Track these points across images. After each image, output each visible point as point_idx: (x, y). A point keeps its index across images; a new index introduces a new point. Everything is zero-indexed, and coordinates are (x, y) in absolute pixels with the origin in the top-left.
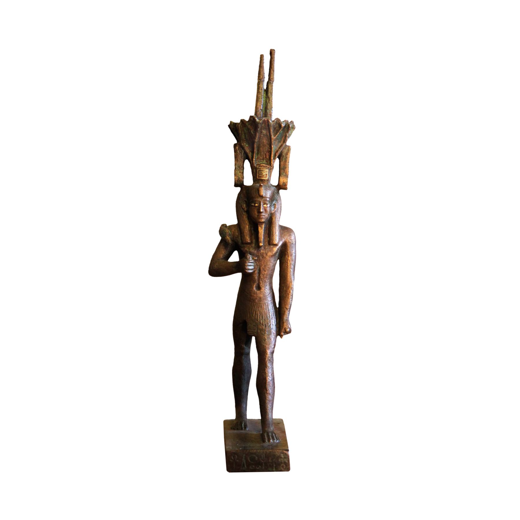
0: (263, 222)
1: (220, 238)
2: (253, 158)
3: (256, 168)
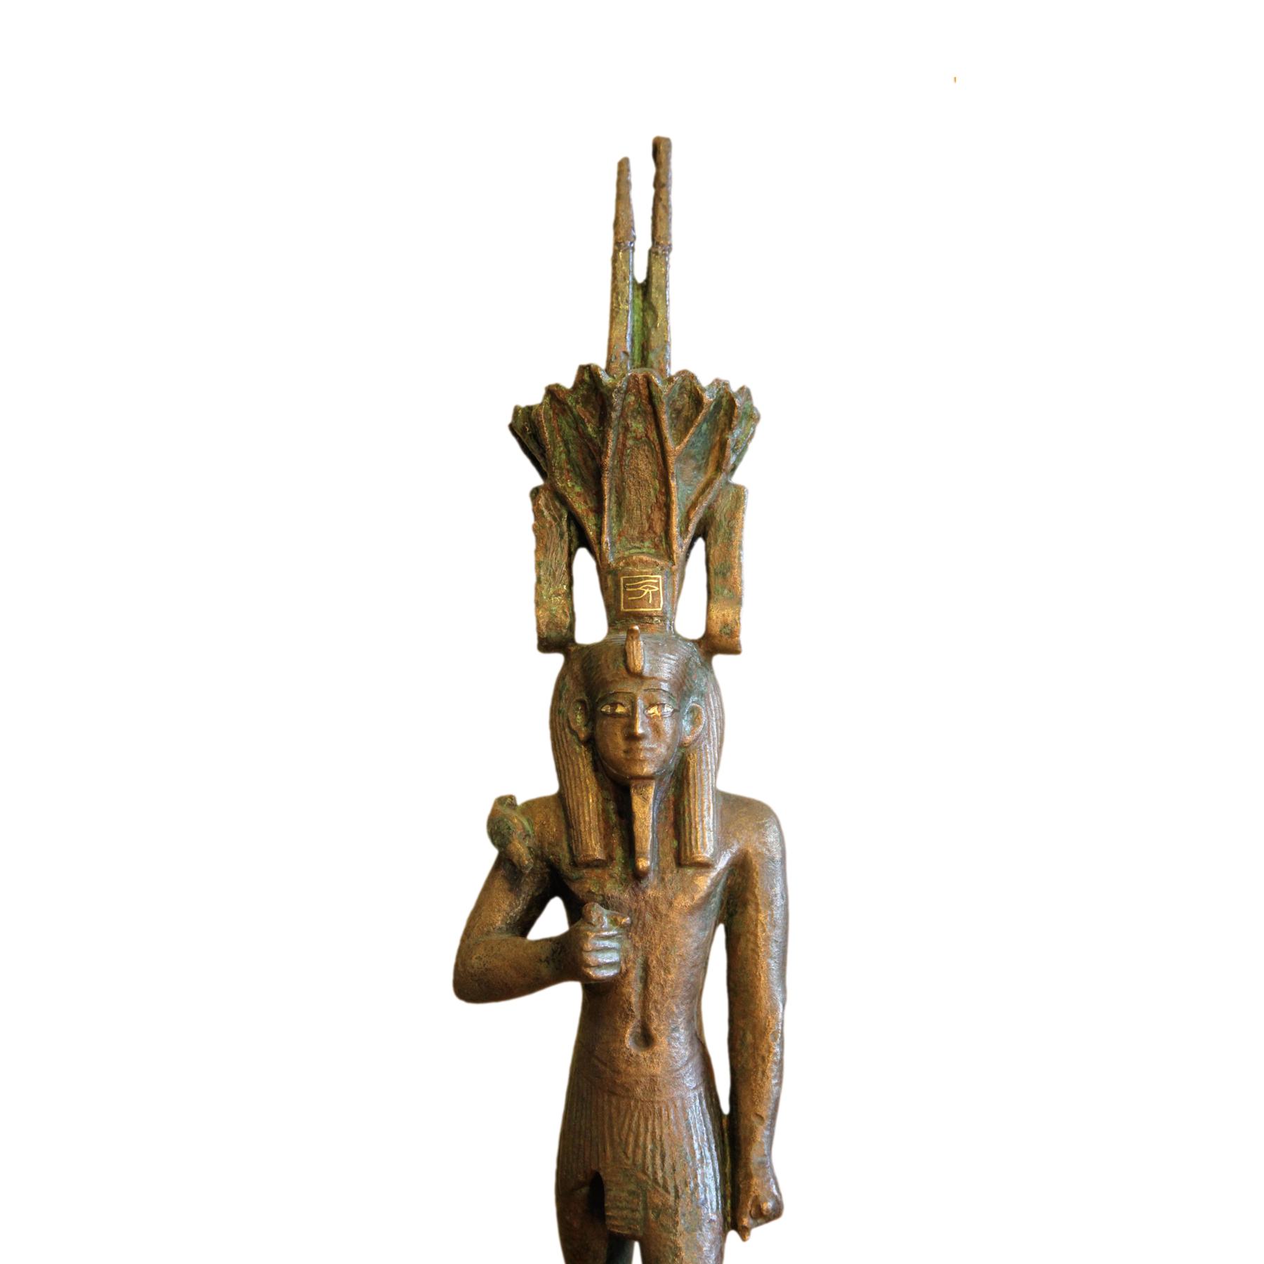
0: (650, 778)
1: (492, 853)
2: (600, 533)
3: (615, 573)
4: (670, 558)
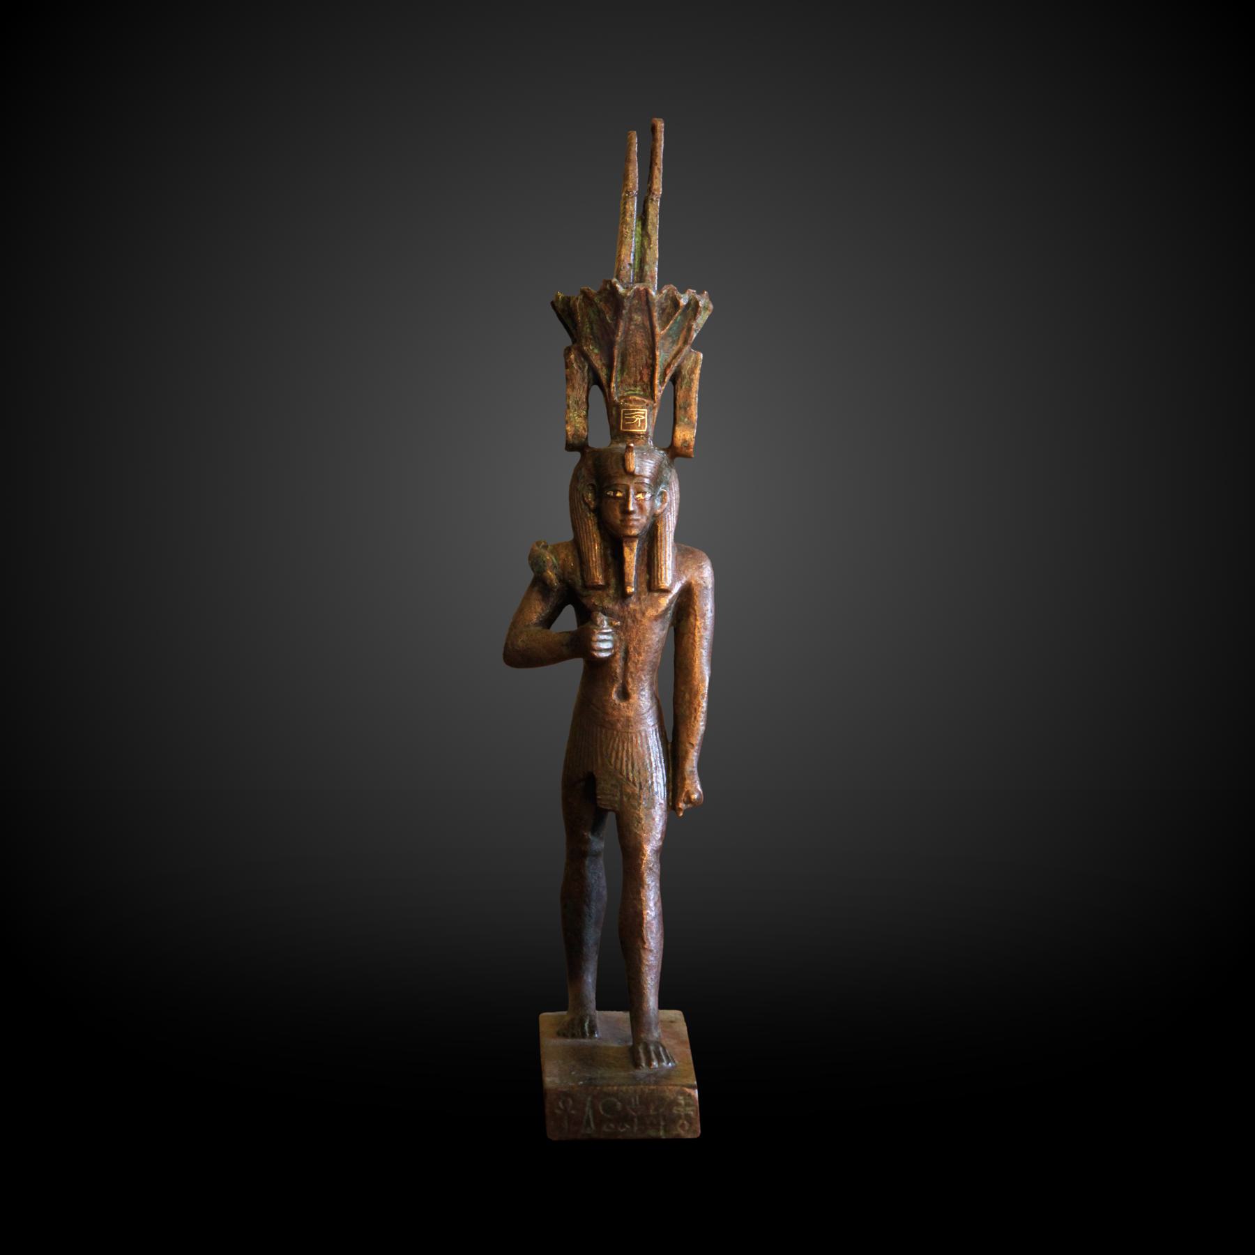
0: (635, 537)
2: (609, 381)
4: (653, 398)
